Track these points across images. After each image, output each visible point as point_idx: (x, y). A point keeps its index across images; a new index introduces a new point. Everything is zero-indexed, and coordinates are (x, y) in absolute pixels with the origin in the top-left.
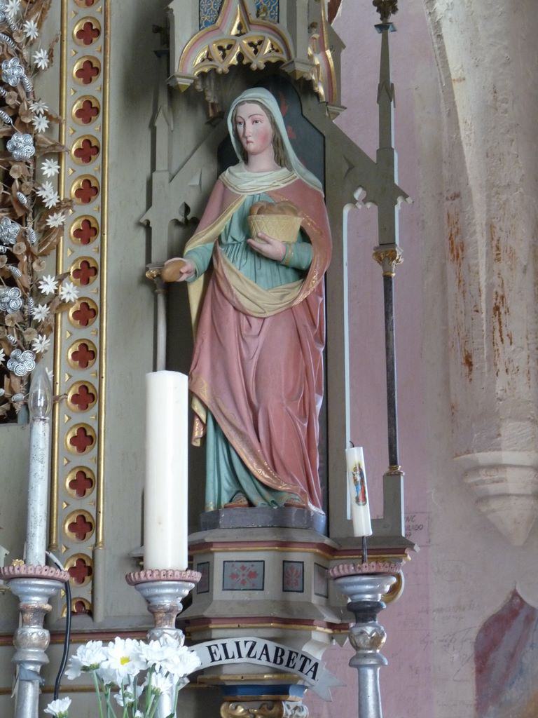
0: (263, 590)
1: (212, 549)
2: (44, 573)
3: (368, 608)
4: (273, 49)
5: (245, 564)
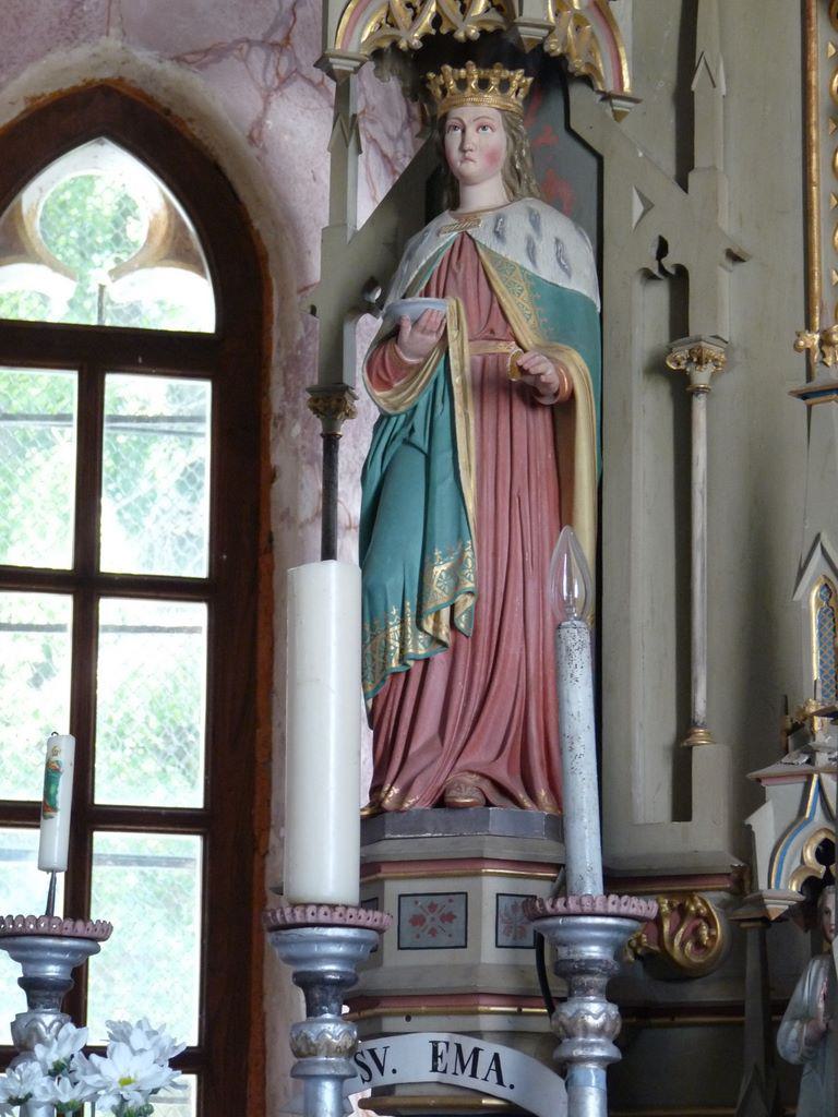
0: (399, 948)
1: (380, 875)
2: (599, 908)
3: (330, 979)
4: (493, 6)
5: (437, 900)
